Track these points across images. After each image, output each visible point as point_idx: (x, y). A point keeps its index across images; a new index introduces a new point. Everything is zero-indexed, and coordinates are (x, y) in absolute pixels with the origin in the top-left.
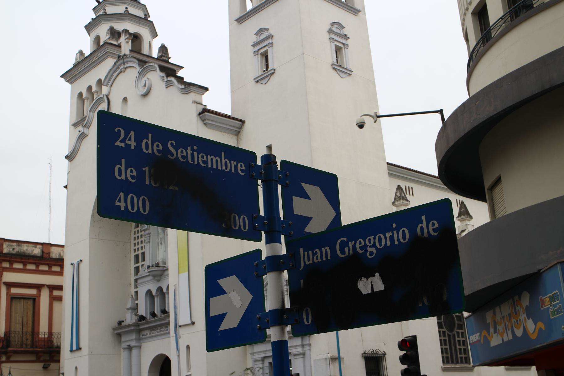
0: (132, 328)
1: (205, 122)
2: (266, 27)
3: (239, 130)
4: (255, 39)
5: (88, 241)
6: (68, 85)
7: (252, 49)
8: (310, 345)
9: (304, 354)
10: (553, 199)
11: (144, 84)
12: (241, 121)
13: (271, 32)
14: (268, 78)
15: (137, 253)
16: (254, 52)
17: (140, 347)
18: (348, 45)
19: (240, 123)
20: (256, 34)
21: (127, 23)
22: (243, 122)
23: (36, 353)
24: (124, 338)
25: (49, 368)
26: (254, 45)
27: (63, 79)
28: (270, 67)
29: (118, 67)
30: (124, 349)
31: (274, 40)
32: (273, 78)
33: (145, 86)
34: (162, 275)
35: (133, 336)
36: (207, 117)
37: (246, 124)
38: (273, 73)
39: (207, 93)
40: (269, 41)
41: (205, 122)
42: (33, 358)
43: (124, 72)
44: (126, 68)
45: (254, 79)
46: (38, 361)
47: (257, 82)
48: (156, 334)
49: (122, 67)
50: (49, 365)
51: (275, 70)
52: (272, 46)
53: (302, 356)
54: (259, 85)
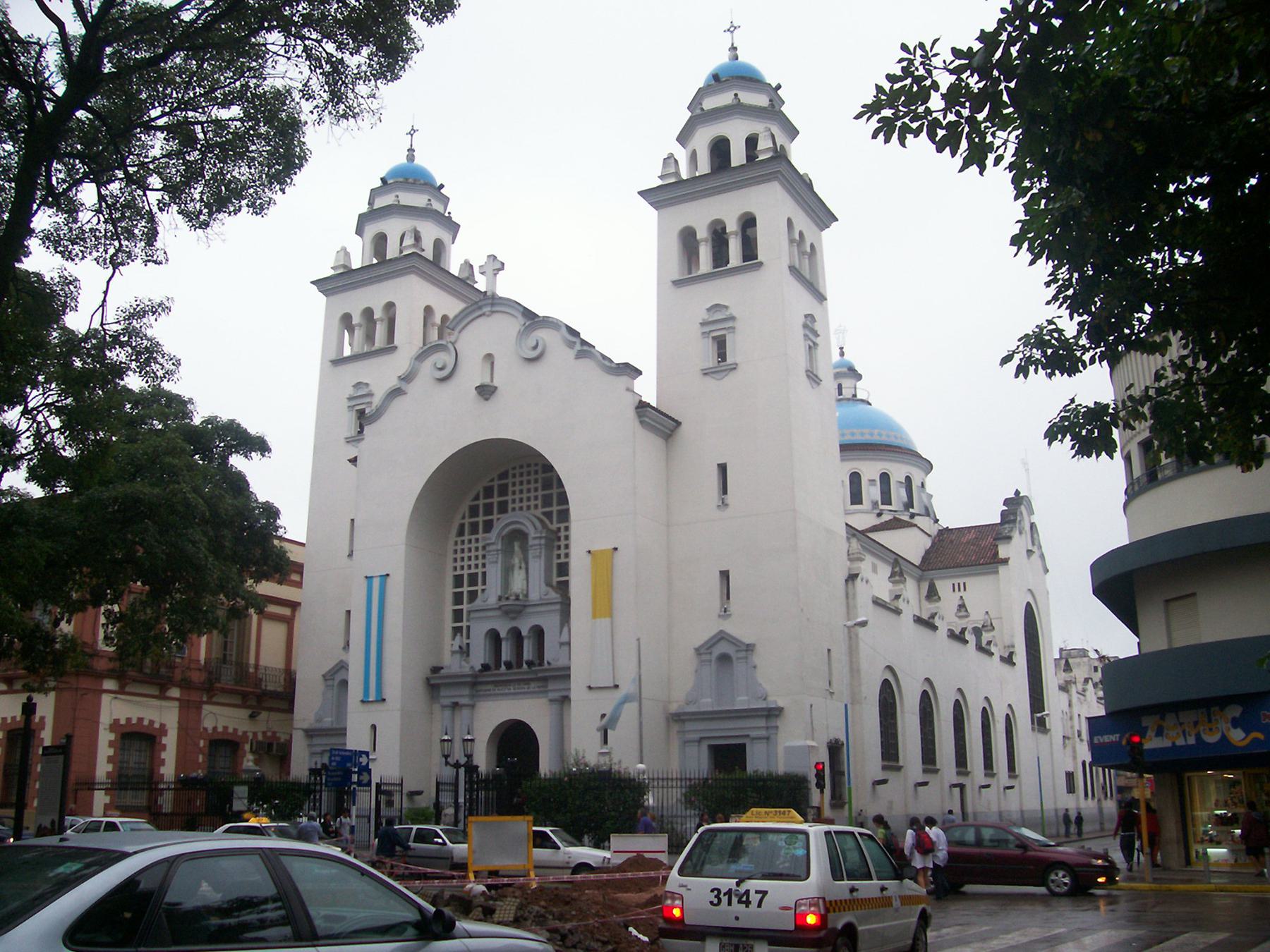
0: (469, 679)
1: (642, 419)
2: (726, 304)
3: (669, 432)
4: (704, 316)
5: (403, 547)
6: (322, 298)
7: (346, 404)
8: (777, 727)
9: (768, 738)
10: (317, 422)
11: (534, 344)
12: (676, 421)
13: (733, 311)
14: (726, 373)
15: (459, 572)
16: (349, 407)
17: (473, 706)
18: (817, 345)
19: (675, 424)
20: (709, 310)
21: (430, 224)
22: (678, 424)
23: (245, 696)
24: (443, 692)
25: (257, 718)
26: (350, 399)
27: (314, 287)
28: (729, 360)
29: (480, 308)
30: (444, 707)
31: (737, 324)
32: (732, 375)
33: (535, 348)
34: (520, 612)
35: (466, 691)
36: (647, 413)
37: (684, 426)
38: (735, 368)
39: (640, 377)
40: (730, 324)
41: (642, 419)
42: (238, 701)
43: (488, 316)
44: (493, 312)
45: (702, 370)
46: (243, 706)
47: (705, 374)
48: (507, 691)
49: (489, 309)
50: (259, 714)
51: (737, 364)
52: (734, 332)
53: (765, 741)
54: (707, 378)
